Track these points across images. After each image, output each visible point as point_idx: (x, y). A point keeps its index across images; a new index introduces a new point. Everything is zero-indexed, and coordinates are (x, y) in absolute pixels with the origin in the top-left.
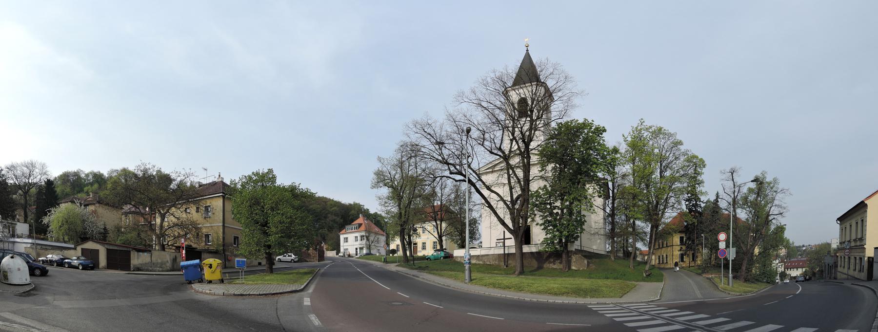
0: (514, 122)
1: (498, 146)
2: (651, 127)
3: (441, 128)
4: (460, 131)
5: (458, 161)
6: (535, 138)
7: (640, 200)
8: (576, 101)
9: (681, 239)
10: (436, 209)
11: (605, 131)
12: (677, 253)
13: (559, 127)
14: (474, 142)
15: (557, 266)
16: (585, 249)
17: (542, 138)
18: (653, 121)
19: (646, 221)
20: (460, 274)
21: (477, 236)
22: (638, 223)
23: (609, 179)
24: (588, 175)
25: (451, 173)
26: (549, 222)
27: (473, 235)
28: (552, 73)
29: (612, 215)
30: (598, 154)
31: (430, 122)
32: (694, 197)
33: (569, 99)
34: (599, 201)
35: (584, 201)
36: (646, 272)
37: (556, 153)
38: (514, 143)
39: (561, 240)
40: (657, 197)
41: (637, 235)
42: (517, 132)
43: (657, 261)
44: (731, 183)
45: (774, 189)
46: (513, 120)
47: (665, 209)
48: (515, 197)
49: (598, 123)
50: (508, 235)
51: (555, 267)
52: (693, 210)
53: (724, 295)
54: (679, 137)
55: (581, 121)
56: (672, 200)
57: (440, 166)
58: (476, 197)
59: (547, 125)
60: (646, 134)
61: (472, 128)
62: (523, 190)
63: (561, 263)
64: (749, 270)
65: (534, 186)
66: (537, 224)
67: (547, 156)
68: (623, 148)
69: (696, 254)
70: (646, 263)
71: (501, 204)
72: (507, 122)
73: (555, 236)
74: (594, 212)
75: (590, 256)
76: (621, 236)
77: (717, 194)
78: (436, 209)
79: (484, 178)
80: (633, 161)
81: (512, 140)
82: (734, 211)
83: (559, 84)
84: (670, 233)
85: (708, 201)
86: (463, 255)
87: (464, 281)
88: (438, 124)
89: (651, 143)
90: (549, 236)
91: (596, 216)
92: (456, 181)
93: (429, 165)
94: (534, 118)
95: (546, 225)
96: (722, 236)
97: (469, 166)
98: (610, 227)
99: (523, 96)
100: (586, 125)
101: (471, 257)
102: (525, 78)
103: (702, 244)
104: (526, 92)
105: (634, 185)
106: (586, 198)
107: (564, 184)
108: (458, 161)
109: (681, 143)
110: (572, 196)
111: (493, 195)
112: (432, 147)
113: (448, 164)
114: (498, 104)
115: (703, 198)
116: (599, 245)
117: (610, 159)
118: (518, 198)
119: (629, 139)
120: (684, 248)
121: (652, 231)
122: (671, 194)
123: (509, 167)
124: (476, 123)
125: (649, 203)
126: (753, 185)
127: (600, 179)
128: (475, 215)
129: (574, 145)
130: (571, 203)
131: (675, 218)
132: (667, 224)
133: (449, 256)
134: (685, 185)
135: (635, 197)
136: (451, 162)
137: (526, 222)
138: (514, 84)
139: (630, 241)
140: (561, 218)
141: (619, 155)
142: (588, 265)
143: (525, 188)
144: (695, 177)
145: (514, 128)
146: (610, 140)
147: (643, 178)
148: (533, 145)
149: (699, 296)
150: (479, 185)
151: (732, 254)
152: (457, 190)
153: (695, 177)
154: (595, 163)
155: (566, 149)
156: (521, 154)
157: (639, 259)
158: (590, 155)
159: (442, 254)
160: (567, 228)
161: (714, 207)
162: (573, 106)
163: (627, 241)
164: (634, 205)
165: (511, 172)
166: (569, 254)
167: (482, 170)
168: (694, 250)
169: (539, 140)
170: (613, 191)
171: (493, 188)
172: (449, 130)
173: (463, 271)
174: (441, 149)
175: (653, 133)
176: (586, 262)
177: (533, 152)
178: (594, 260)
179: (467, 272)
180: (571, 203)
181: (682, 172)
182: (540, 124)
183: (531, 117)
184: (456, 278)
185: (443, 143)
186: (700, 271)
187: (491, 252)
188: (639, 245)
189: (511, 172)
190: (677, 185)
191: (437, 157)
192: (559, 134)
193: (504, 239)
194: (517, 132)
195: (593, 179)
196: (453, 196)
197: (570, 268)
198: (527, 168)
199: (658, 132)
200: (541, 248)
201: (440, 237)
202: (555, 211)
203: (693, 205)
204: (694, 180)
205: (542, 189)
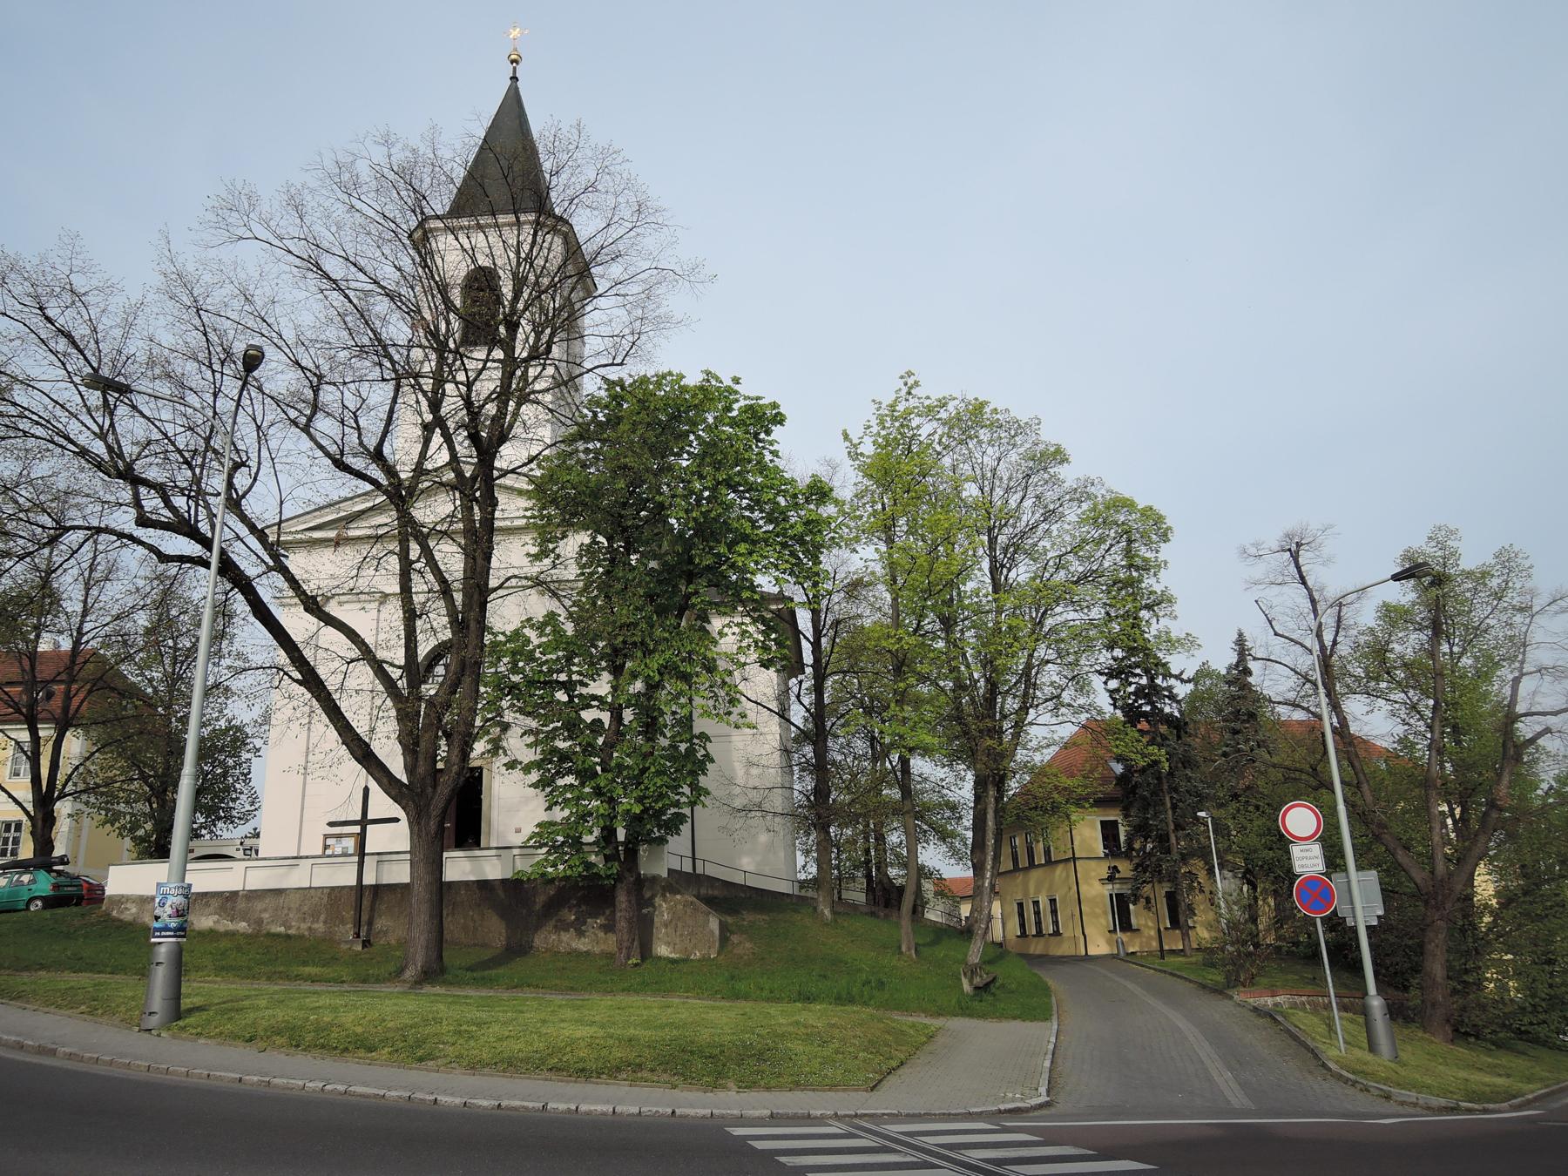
0: (441, 360)
1: (371, 443)
2: (943, 404)
3: (128, 326)
4: (215, 355)
5: (184, 476)
6: (518, 430)
7: (923, 678)
8: (674, 301)
9: (1109, 830)
10: (44, 672)
11: (779, 419)
12: (1097, 890)
13: (614, 397)
14: (273, 413)
15: (593, 940)
16: (712, 871)
17: (546, 433)
18: (948, 382)
19: (953, 758)
20: (123, 986)
21: (242, 805)
22: (919, 765)
23: (799, 596)
24: (719, 581)
25: (143, 521)
26: (564, 756)
27: (217, 799)
28: (591, 187)
29: (817, 734)
30: (757, 504)
31: (79, 283)
32: (1137, 661)
33: (648, 293)
34: (761, 683)
35: (703, 680)
36: (972, 972)
37: (596, 494)
38: (437, 438)
39: (608, 834)
40: (987, 663)
41: (922, 815)
42: (452, 403)
43: (1014, 924)
44: (1298, 595)
45: (1512, 598)
46: (441, 348)
47: (1024, 709)
48: (423, 650)
49: (755, 387)
50: (381, 804)
51: (582, 945)
52: (1141, 708)
53: (1362, 1102)
54: (1050, 435)
55: (693, 379)
56: (1051, 675)
57: (93, 481)
58: (251, 636)
59: (566, 383)
60: (926, 429)
61: (270, 352)
62: (458, 624)
63: (609, 928)
64: (1464, 980)
65: (507, 614)
66: (511, 765)
67: (562, 502)
68: (847, 482)
69: (1186, 899)
70: (966, 933)
71: (363, 675)
72: (417, 354)
73: (584, 816)
74: (743, 723)
75: (731, 900)
76: (852, 820)
77: (1240, 641)
78: (44, 672)
79: (297, 562)
80: (887, 530)
81: (428, 429)
82: (1335, 707)
83: (615, 232)
84: (1055, 808)
85: (1204, 673)
86: (150, 891)
87: (136, 1021)
88: (117, 303)
89: (947, 461)
90: (559, 814)
91: (751, 738)
92: (164, 558)
93: (41, 469)
94: (521, 352)
95: (549, 769)
96: (1300, 820)
97: (234, 504)
98: (809, 783)
99: (483, 261)
100: (710, 394)
101: (193, 901)
102: (498, 193)
103: (1204, 854)
104: (494, 245)
105: (897, 623)
106: (710, 668)
107: (623, 613)
108: (184, 476)
109: (1059, 456)
110: (655, 662)
111: (330, 635)
112: (69, 395)
113: (136, 481)
114: (389, 275)
115: (1178, 662)
116: (771, 857)
117: (800, 530)
118: (435, 656)
119: (868, 448)
120: (1125, 868)
121: (978, 798)
122: (1042, 651)
123: (409, 530)
124: (291, 340)
125: (960, 686)
126: (1403, 595)
127: (766, 598)
128: (240, 712)
129: (670, 468)
130: (653, 687)
131: (1067, 746)
132: (1039, 773)
133: (78, 896)
134: (1097, 613)
135: (901, 665)
136: (153, 474)
137: (465, 756)
138: (457, 210)
139: (894, 838)
140: (610, 746)
141: (829, 510)
142: (724, 939)
143: (470, 618)
144: (1130, 583)
145: (439, 381)
146: (799, 452)
147: (929, 592)
148: (509, 455)
149: (1238, 1099)
150: (269, 588)
151: (1362, 900)
152: (165, 599)
153: (1130, 583)
154: (745, 538)
155: (636, 482)
156: (461, 485)
157: (934, 915)
158: (729, 506)
159: (44, 884)
160: (639, 781)
161: (1237, 697)
162: (662, 322)
163: (881, 838)
164: (902, 698)
165: (415, 550)
166: (643, 888)
167: (292, 531)
168: (1173, 878)
169: (531, 440)
170: (816, 645)
171: (332, 609)
172: (167, 339)
173: (144, 973)
174: (109, 410)
175: (949, 424)
176: (714, 924)
177: (508, 481)
178: (748, 917)
179: (160, 975)
180: (653, 687)
181: (1077, 567)
182: (541, 378)
183: (509, 347)
184: (96, 1006)
185: (124, 390)
186: (1216, 977)
187: (298, 878)
188: (932, 855)
189: (415, 550)
190: (1063, 615)
191: (84, 439)
192: (614, 421)
193: (364, 822)
194: (452, 403)
195: (738, 596)
196: (143, 619)
197: (646, 952)
198: (479, 541)
199: (972, 420)
200: (524, 865)
201: (45, 801)
202: (588, 716)
203: (1139, 692)
204: (1131, 594)
205: (540, 628)
